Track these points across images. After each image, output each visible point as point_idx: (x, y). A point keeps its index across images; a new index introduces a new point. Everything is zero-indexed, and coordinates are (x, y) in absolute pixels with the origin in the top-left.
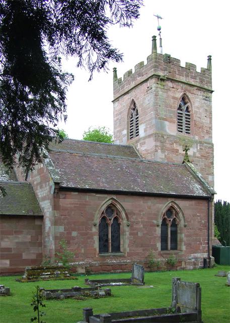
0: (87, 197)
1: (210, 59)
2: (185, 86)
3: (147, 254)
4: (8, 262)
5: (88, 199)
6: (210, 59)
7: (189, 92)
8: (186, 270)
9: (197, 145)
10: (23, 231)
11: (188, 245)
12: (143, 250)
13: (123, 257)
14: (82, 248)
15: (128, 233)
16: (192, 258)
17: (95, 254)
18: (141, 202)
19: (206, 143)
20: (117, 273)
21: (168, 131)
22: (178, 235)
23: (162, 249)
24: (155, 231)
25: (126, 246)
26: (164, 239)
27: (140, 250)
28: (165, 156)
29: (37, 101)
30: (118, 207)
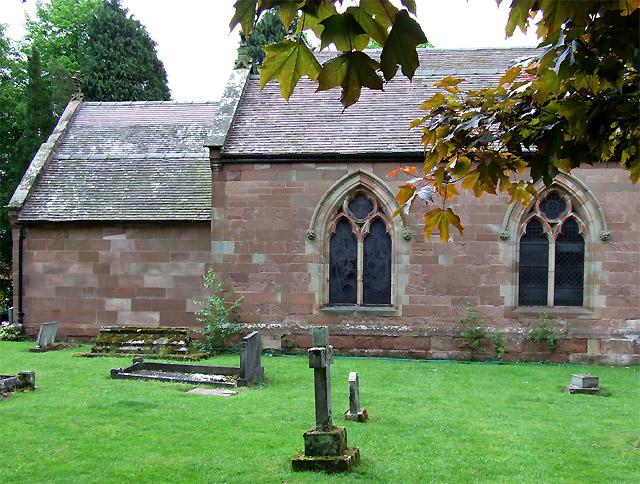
0: (294, 175)
3: (465, 312)
4: (156, 316)
5: (294, 179)
8: (603, 365)
10: (188, 254)
11: (616, 294)
12: (454, 303)
13: (392, 316)
14: (277, 291)
15: (406, 259)
16: (630, 333)
17: (311, 306)
20: (368, 355)
22: (586, 264)
23: (523, 300)
24: (495, 252)
25: (402, 290)
26: (530, 277)
27: (444, 301)
29: (625, 134)
30: (379, 192)
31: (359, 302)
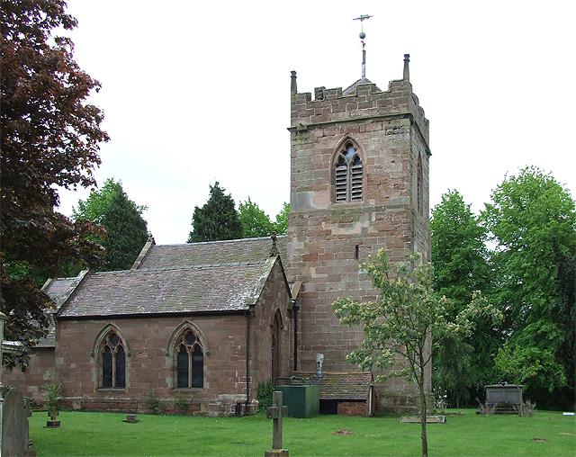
1: (407, 59)
2: (345, 126)
6: (407, 59)
7: (354, 131)
9: (370, 214)
11: (214, 381)
18: (144, 326)
19: (389, 207)
21: (312, 205)
24: (164, 362)
26: (181, 371)
27: (144, 386)
28: (305, 244)
31: (190, 385)
